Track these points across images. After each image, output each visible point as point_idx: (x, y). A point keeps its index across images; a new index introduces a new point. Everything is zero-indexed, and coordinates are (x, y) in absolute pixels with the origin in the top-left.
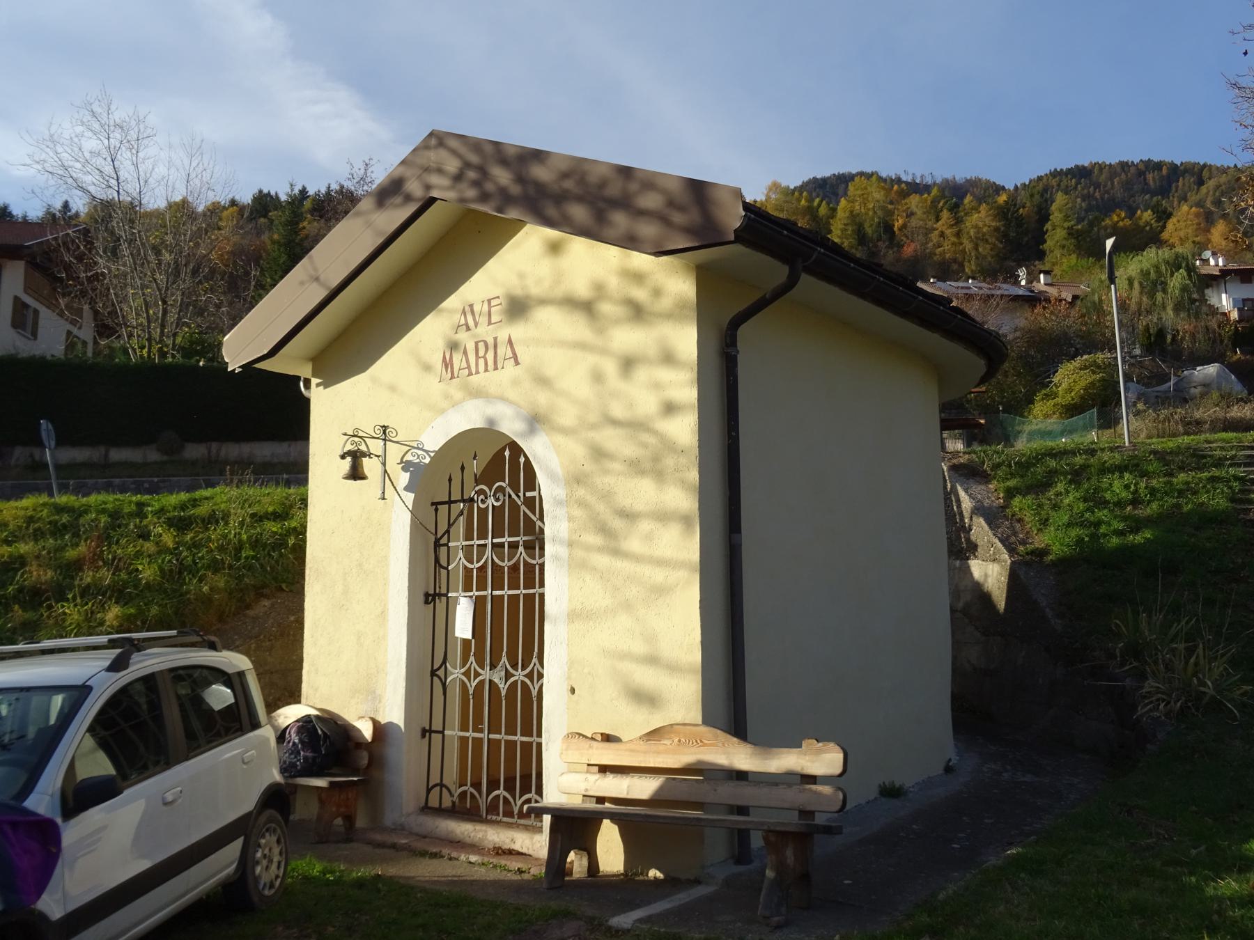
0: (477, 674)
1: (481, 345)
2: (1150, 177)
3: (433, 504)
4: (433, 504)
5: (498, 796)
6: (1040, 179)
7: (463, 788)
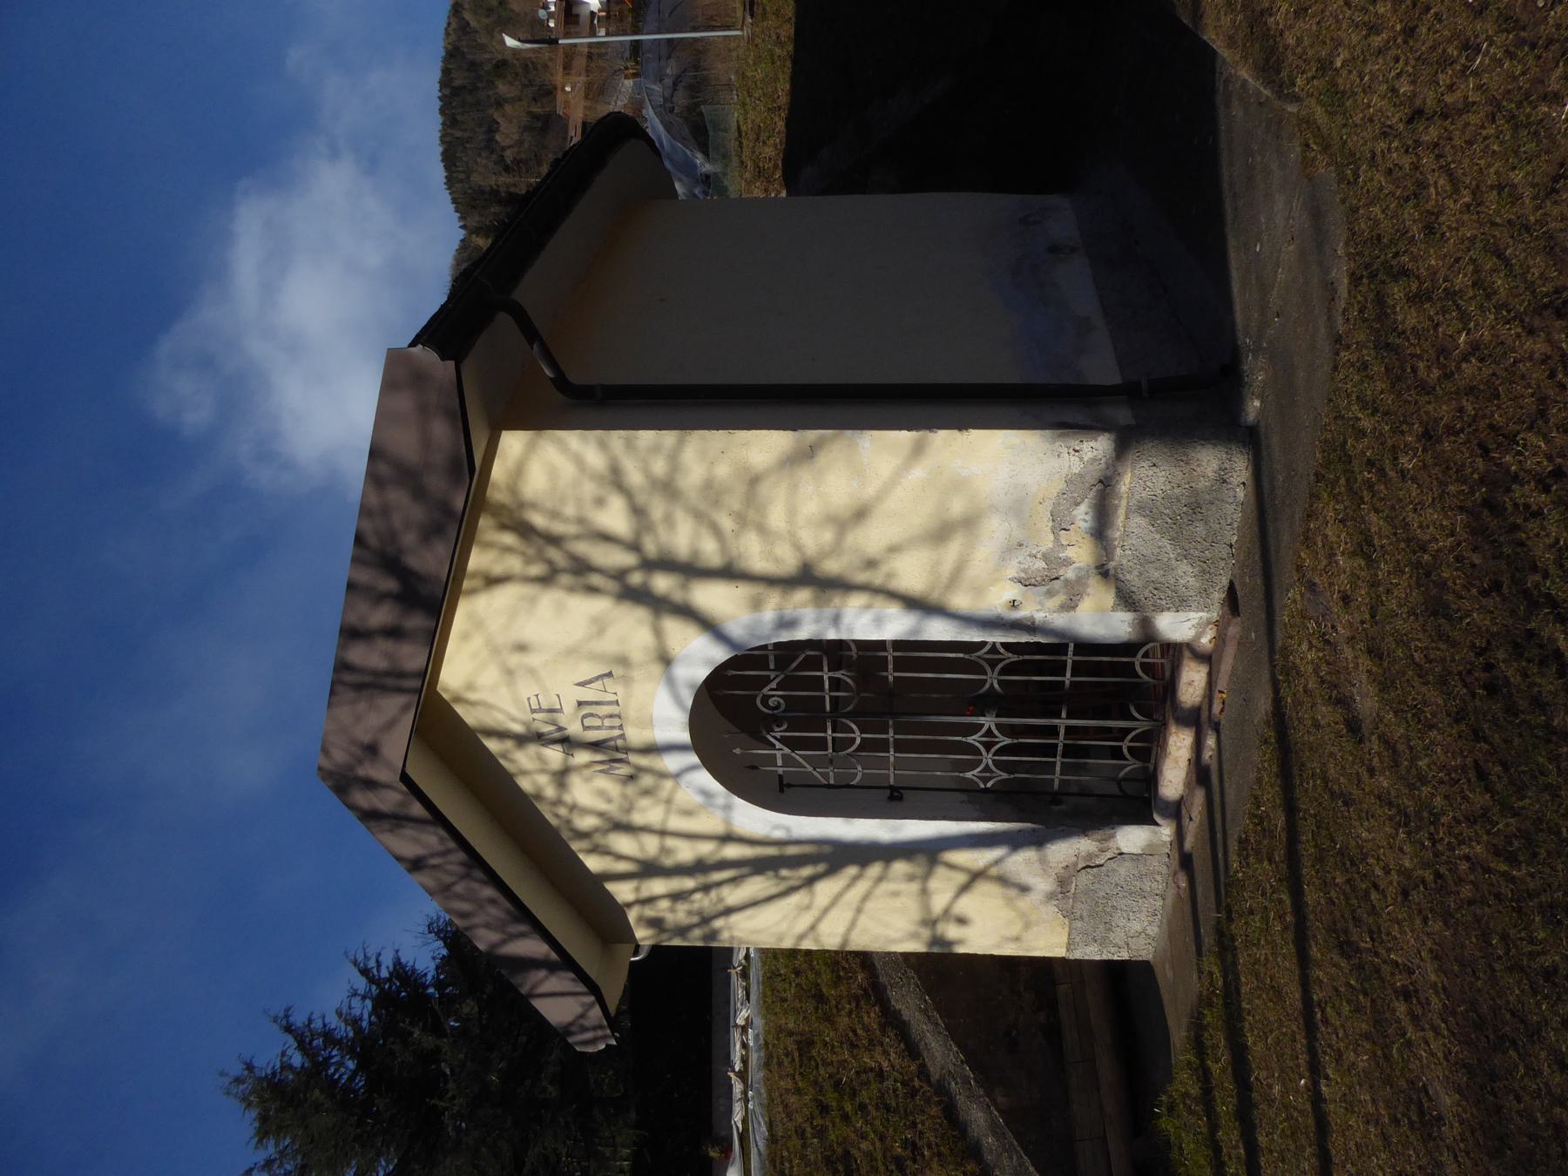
0: (989, 733)
1: (588, 722)
2: (457, 83)
3: (781, 790)
4: (781, 790)
5: (1129, 748)
6: (454, 201)
7: (1125, 751)
